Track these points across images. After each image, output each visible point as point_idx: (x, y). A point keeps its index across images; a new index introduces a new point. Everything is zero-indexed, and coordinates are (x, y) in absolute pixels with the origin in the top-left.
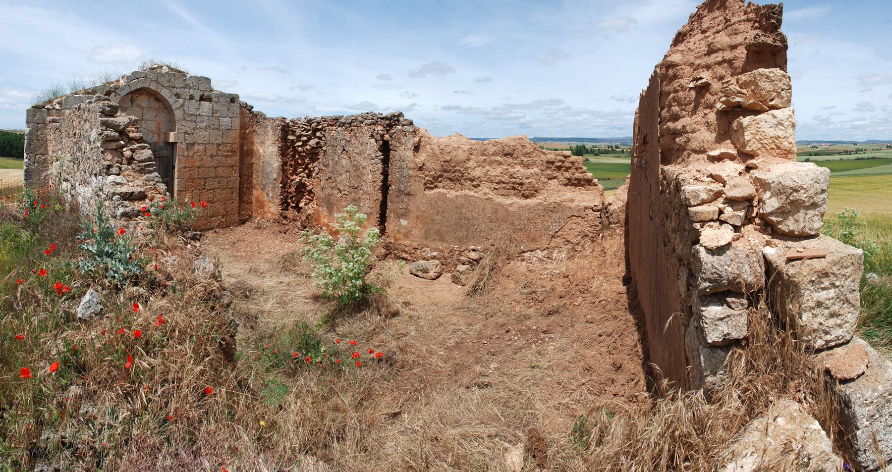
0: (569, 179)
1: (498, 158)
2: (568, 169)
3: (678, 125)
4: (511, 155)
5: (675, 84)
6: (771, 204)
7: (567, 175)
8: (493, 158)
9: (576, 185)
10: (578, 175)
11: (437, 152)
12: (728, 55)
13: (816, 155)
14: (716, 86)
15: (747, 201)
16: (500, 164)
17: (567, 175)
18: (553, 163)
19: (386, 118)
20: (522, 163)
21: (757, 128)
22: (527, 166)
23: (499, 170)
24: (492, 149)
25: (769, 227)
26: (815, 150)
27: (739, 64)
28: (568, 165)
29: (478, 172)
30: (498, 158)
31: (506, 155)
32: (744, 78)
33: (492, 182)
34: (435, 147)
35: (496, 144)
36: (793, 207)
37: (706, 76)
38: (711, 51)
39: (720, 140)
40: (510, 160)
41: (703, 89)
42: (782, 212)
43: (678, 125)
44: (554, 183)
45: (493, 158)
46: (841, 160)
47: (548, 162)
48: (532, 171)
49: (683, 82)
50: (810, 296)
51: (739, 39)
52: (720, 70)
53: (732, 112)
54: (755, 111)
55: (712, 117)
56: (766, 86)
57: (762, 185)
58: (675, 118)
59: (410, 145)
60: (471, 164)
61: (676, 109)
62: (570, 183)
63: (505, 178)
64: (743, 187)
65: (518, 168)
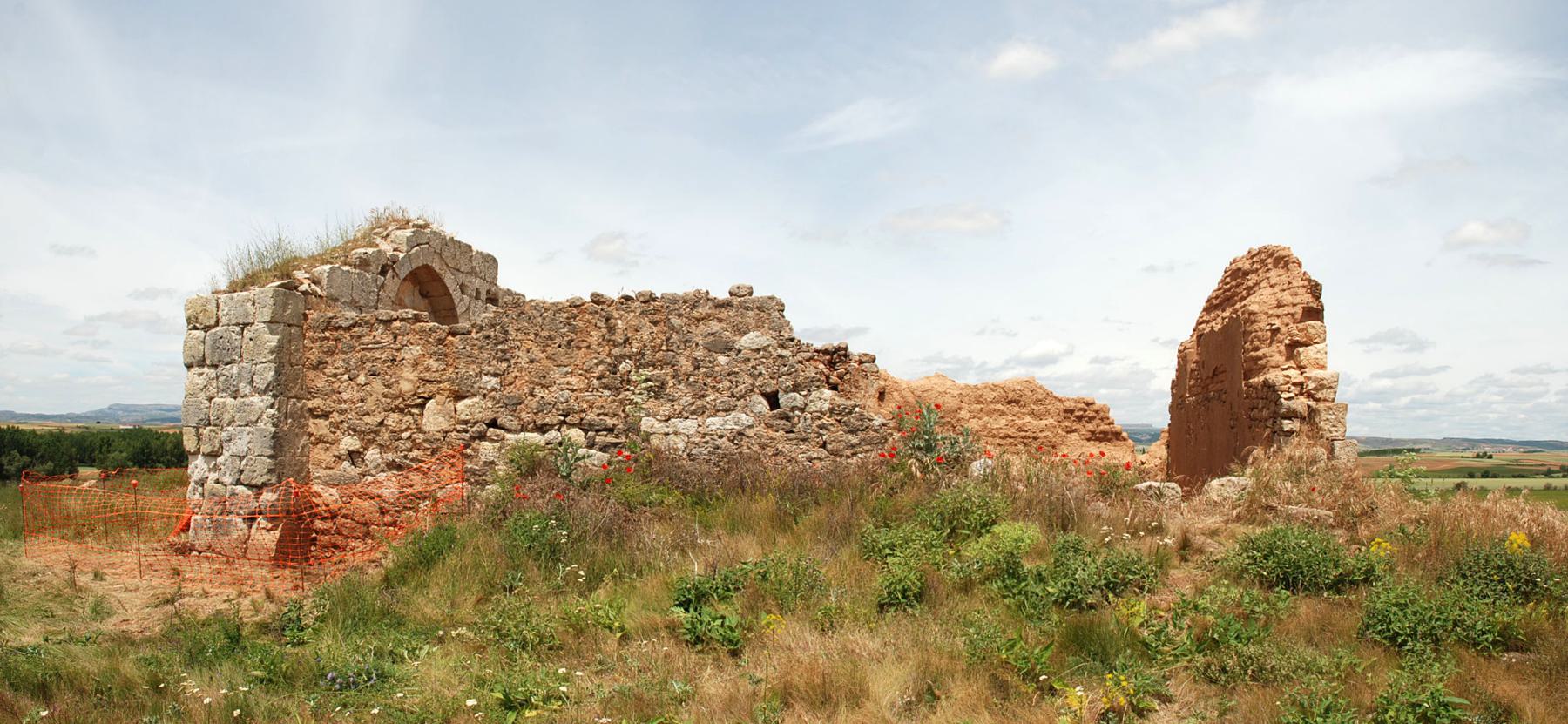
0: (1093, 433)
1: (999, 407)
2: (1091, 419)
3: (1260, 353)
4: (1017, 402)
5: (1255, 326)
6: (1311, 385)
7: (1090, 427)
8: (992, 406)
9: (1100, 440)
10: (1103, 427)
11: (911, 399)
12: (1291, 310)
13: (1486, 474)
14: (1284, 329)
15: (1301, 384)
16: (1002, 413)
17: (1090, 427)
18: (1072, 412)
19: (826, 352)
20: (1032, 413)
21: (1307, 354)
22: (1040, 417)
23: (1002, 422)
24: (992, 395)
25: (1310, 396)
26: (1486, 462)
27: (1298, 316)
28: (1091, 414)
29: (974, 425)
30: (999, 407)
31: (1009, 402)
32: (1301, 326)
33: (994, 436)
34: (907, 394)
35: (994, 388)
36: (1321, 387)
37: (1277, 323)
38: (1279, 306)
39: (1288, 359)
40: (1017, 409)
41: (1276, 331)
42: (1316, 389)
43: (1260, 353)
44: (1074, 436)
45: (992, 406)
46: (1548, 488)
47: (1066, 411)
48: (1044, 422)
49: (1262, 325)
50: (1324, 416)
51: (1298, 300)
52: (1287, 320)
53: (1294, 346)
54: (1306, 345)
55: (1282, 348)
56: (1312, 331)
57: (1309, 378)
58: (1257, 349)
59: (873, 391)
60: (963, 414)
61: (1256, 343)
62: (1095, 437)
63: (1012, 432)
64: (1301, 379)
65: (1028, 419)
